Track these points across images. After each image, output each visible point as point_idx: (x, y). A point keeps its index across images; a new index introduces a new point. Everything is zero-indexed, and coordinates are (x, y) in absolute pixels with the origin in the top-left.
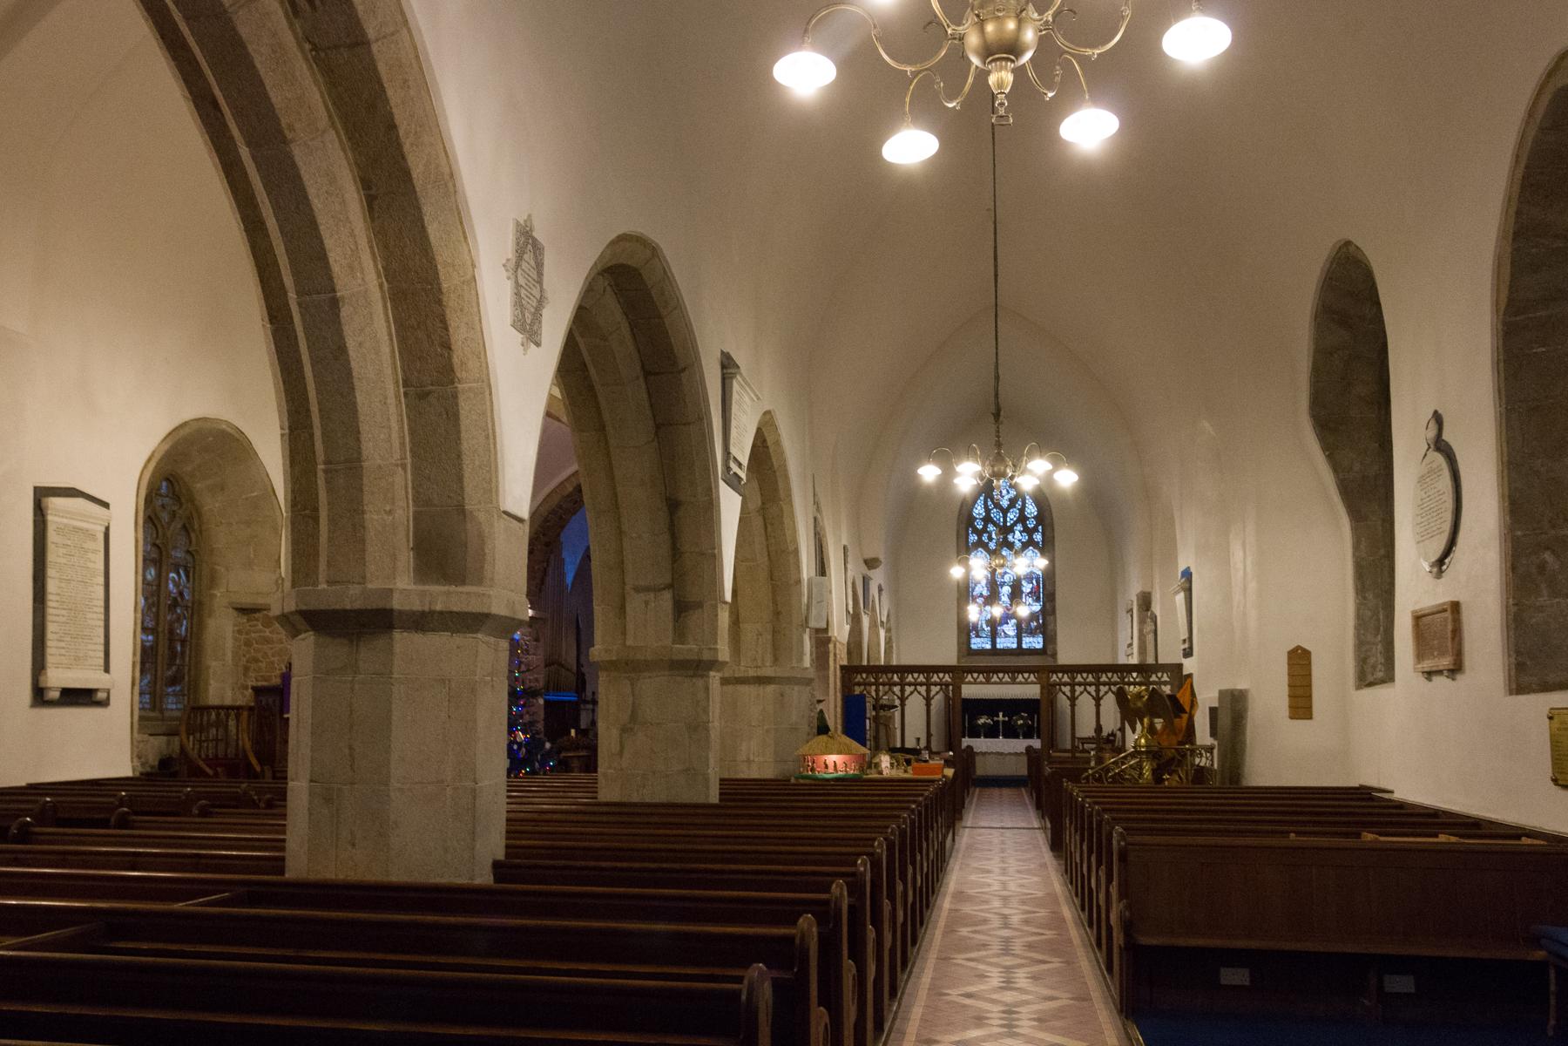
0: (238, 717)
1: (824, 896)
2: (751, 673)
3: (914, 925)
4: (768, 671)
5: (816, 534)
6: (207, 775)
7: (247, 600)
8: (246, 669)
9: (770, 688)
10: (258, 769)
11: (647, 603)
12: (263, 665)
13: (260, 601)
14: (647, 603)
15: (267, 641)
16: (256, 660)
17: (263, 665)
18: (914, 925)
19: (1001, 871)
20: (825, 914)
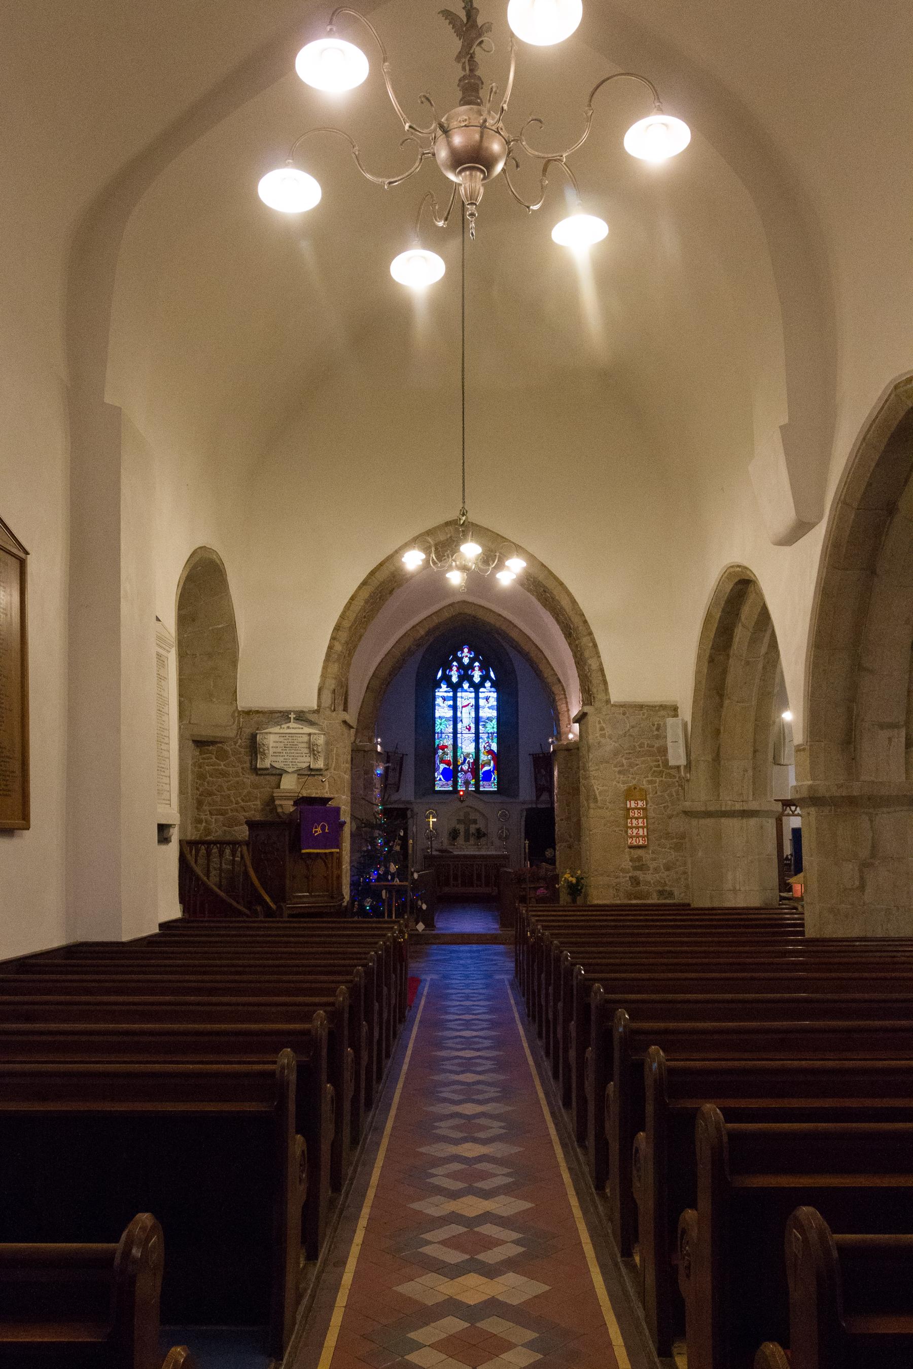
0: (221, 853)
1: (307, 1026)
2: (738, 807)
3: (388, 1039)
4: (754, 805)
5: (208, 742)
6: (241, 914)
7: (206, 732)
8: (200, 803)
9: (753, 821)
10: (273, 906)
11: (890, 739)
12: (218, 799)
13: (219, 733)
14: (890, 739)
15: (224, 774)
16: (210, 794)
17: (218, 798)
18: (388, 1039)
19: (466, 984)
20: (303, 1043)
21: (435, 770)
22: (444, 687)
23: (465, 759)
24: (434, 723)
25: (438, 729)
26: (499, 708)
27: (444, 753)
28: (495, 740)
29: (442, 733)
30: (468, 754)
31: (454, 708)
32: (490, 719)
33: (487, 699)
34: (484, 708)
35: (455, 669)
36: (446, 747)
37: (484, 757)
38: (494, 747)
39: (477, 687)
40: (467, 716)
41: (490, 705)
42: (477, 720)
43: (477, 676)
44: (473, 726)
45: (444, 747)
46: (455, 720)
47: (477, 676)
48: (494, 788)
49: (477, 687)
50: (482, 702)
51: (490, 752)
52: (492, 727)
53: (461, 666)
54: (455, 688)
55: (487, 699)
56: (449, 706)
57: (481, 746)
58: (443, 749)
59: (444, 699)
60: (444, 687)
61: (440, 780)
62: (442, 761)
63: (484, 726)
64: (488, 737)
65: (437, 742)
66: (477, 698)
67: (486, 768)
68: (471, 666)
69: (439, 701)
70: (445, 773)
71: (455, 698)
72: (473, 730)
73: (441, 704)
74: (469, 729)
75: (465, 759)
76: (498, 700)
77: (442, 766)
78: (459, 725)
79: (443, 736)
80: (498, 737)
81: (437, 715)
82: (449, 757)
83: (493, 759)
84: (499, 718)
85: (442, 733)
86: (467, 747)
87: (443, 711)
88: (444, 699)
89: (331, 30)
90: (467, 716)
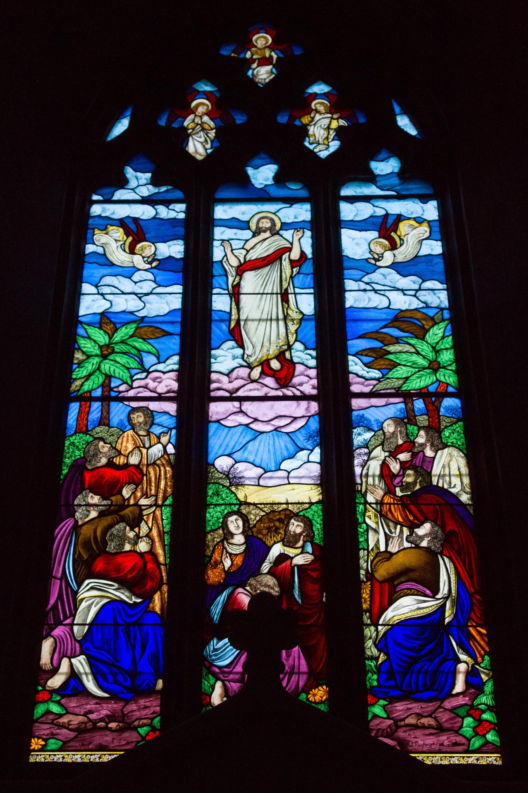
21: (43, 614)
22: (139, 181)
23: (256, 549)
24: (70, 345)
25: (86, 376)
26: (455, 268)
27: (121, 514)
28: (453, 433)
29: (108, 397)
30: (278, 518)
31: (196, 273)
32: (412, 323)
33: (387, 228)
34: (370, 265)
35: (201, 105)
36: (136, 475)
37: (381, 538)
38: (451, 468)
39: (320, 185)
40: (264, 314)
41: (404, 253)
42: (331, 328)
43: (322, 133)
44: (304, 357)
45: (113, 479)
46: (196, 331)
47: (322, 133)
48: (315, 576)
49: (320, 185)
50: (355, 244)
51: (424, 501)
52: (428, 361)
53: (234, 91)
54: (201, 188)
55: (387, 228)
56: (163, 265)
57: (369, 467)
58: (108, 488)
59: (136, 232)
60: (139, 181)
61: (73, 686)
62: (95, 561)
63: (378, 358)
64: (407, 419)
65: (74, 447)
66: (326, 228)
67: (406, 607)
68: (289, 92)
69: (110, 242)
70: (105, 640)
71: (198, 231)
72: (306, 381)
73: (119, 257)
74: (285, 374)
75: (256, 549)
76: (444, 228)
77: (92, 598)
78: (224, 359)
79: (118, 412)
80: (467, 416)
81: (90, 304)
82: (148, 538)
83: (448, 544)
84: (461, 316)
85: (108, 397)
86: (270, 468)
87: (124, 284)
88: (136, 232)
89: (403, 437)
90: (264, 314)
